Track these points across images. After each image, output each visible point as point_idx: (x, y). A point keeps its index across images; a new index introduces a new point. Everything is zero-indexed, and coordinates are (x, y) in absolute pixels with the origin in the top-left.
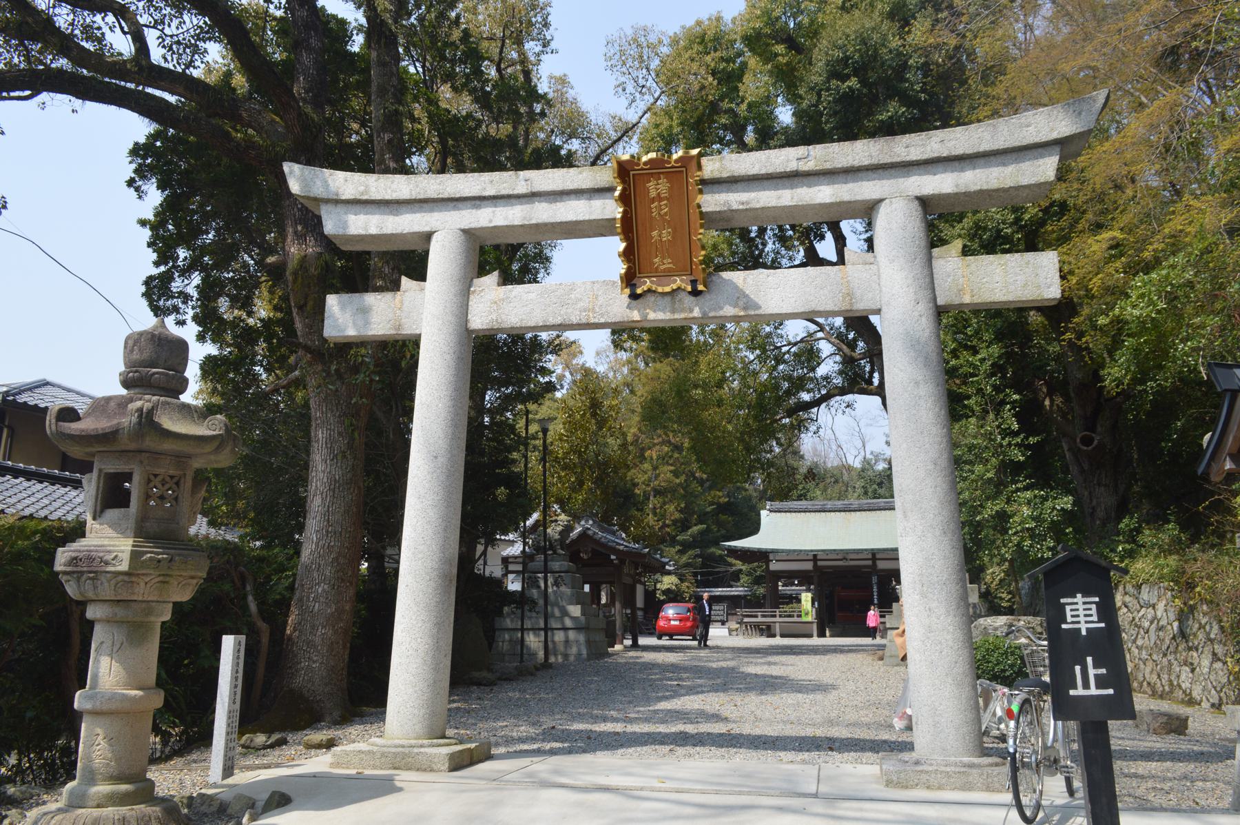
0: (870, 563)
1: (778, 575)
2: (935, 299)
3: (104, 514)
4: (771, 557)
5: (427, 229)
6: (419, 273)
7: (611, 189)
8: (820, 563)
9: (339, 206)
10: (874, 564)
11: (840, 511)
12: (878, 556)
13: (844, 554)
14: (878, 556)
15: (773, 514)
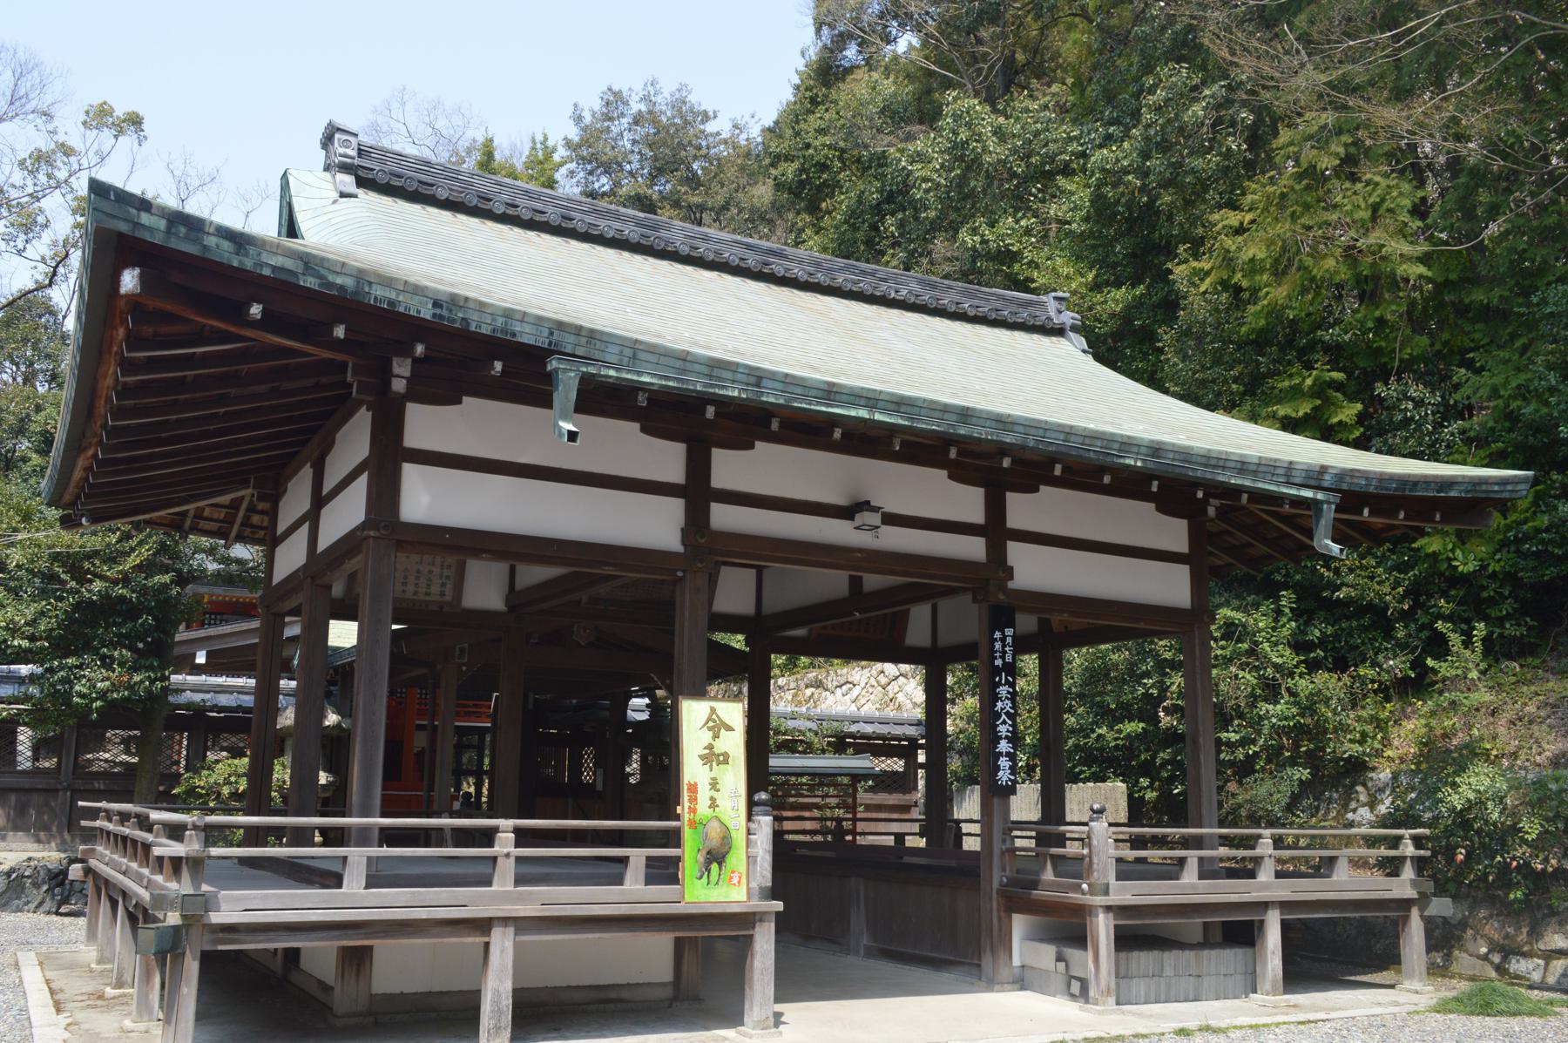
0: (973, 548)
8: (723, 517)
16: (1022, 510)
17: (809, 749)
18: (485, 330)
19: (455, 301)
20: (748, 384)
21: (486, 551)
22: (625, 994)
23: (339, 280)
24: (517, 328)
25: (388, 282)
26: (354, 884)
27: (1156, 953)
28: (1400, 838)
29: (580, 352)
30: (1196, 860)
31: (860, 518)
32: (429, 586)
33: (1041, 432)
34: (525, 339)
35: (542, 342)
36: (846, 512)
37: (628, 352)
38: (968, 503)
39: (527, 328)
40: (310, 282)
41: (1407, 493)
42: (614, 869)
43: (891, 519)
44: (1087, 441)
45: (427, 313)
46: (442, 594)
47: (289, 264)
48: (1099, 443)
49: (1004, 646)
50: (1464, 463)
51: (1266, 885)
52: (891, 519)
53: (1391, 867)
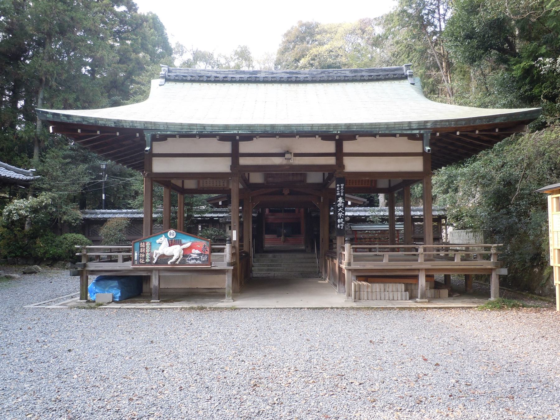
0: (332, 161)
8: (243, 161)
10: (340, 164)
16: (348, 146)
17: (372, 222)
18: (128, 127)
19: (119, 121)
20: (201, 129)
21: (175, 178)
22: (217, 291)
23: (91, 121)
24: (136, 125)
25: (102, 119)
26: (386, 260)
27: (394, 285)
28: (491, 247)
29: (153, 128)
30: (387, 256)
31: (287, 156)
32: (220, 183)
33: (302, 128)
34: (139, 127)
35: (143, 127)
36: (282, 155)
37: (166, 126)
38: (330, 147)
39: (138, 125)
40: (85, 123)
41: (471, 124)
42: (381, 258)
43: (296, 155)
44: (320, 128)
45: (113, 125)
46: (224, 185)
47: (79, 119)
48: (325, 128)
49: (340, 189)
50: (525, 107)
51: (421, 263)
52: (296, 155)
53: (488, 257)
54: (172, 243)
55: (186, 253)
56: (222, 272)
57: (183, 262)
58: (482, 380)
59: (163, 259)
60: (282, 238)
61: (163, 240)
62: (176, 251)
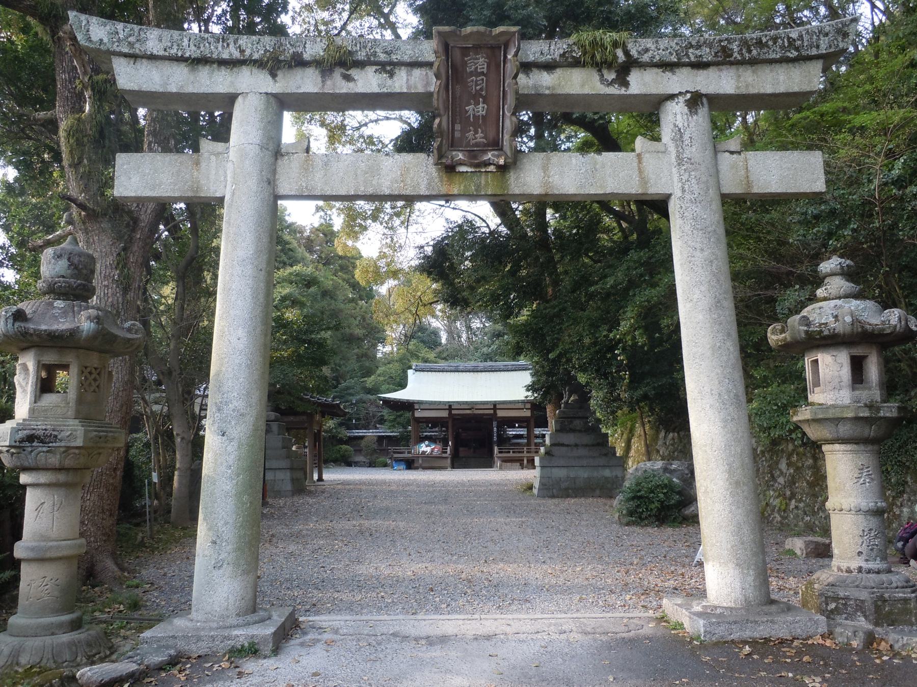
0: (492, 412)
1: (419, 421)
2: (719, 188)
3: (42, 399)
4: (416, 406)
5: (232, 90)
6: (221, 133)
7: (429, 65)
8: (453, 412)
9: (139, 61)
10: (495, 413)
11: (470, 371)
12: (498, 407)
13: (472, 405)
14: (498, 407)
15: (418, 373)
54: (427, 446)
55: (432, 450)
56: (446, 458)
57: (431, 454)
58: (779, 227)
59: (424, 452)
60: (472, 450)
61: (423, 445)
62: (428, 450)
